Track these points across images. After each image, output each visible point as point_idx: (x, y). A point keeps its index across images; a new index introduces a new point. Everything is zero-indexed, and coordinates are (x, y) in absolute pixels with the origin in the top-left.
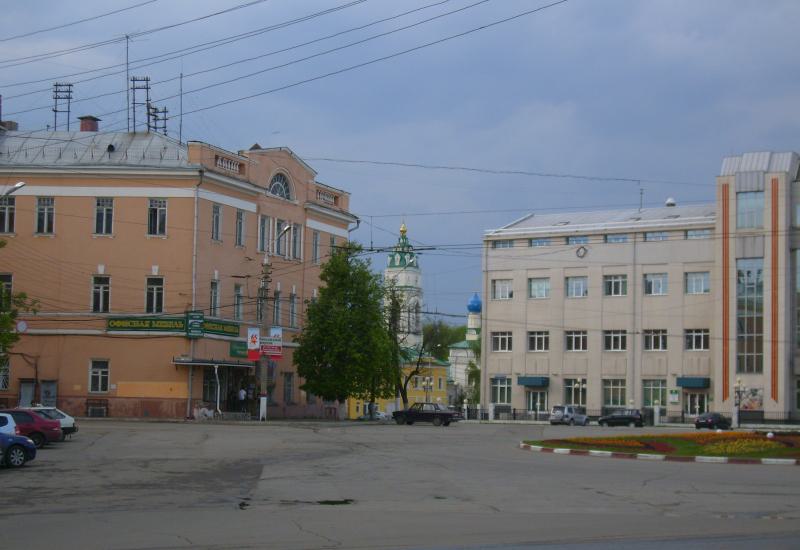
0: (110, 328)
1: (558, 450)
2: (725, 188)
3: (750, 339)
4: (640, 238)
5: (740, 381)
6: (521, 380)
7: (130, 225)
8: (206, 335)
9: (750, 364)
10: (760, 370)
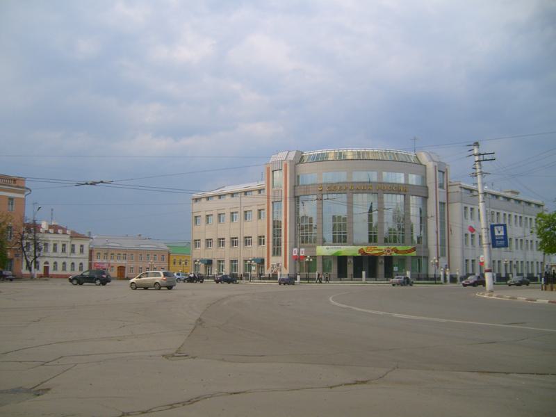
4: (243, 195)
5: (274, 260)
9: (277, 252)
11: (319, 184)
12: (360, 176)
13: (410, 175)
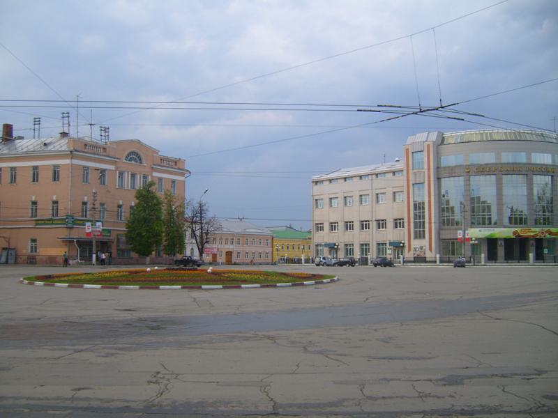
0: (37, 224)
1: (37, 283)
2: (407, 150)
3: (420, 222)
4: (374, 176)
5: (416, 243)
6: (391, 244)
7: (45, 176)
8: (75, 226)
9: (420, 235)
10: (424, 237)
11: (466, 165)
12: (508, 158)
13: (533, 154)
